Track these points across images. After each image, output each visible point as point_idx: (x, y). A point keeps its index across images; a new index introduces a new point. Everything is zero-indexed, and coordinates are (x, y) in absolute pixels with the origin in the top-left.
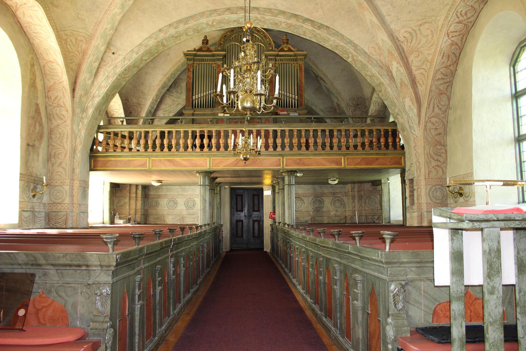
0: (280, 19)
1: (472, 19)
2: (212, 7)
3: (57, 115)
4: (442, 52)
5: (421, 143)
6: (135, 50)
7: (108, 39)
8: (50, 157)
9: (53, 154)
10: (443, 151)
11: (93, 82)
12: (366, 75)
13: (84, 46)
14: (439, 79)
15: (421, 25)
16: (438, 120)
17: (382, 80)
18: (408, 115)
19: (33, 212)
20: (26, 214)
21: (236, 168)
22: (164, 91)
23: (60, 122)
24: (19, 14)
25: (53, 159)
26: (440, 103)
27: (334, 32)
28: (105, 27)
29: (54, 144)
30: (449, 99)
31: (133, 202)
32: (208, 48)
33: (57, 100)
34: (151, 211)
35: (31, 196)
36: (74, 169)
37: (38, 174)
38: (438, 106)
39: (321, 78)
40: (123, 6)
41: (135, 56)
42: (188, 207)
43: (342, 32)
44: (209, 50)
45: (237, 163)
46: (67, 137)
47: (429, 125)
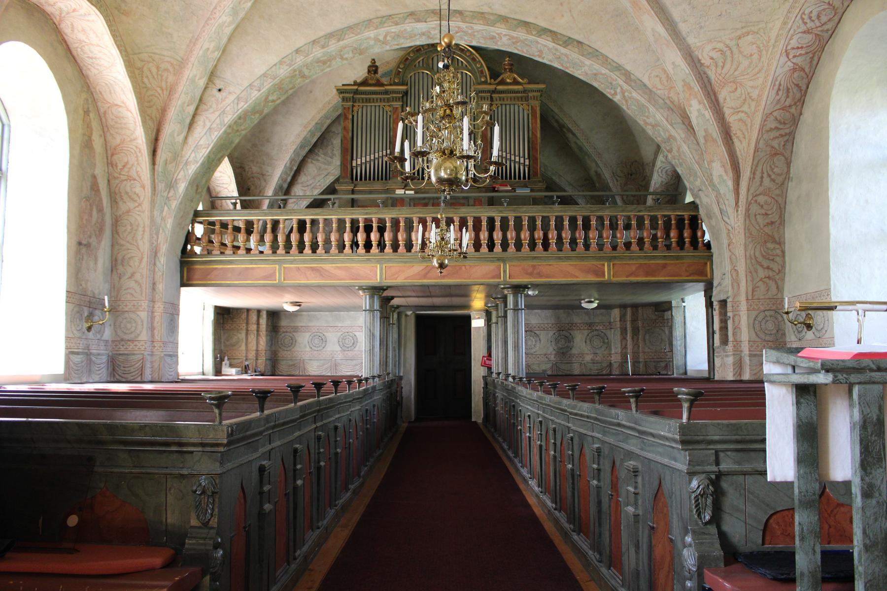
0: (499, 31)
1: (829, 26)
2: (384, 11)
3: (127, 193)
4: (777, 83)
5: (739, 239)
6: (255, 84)
7: (210, 66)
8: (115, 264)
9: (120, 258)
10: (778, 252)
11: (186, 138)
12: (646, 123)
13: (171, 79)
14: (771, 130)
15: (740, 38)
16: (769, 200)
17: (673, 132)
18: (718, 191)
19: (88, 355)
20: (76, 359)
21: (426, 281)
22: (304, 153)
23: (132, 205)
24: (65, 28)
25: (120, 267)
26: (772, 170)
27: (591, 50)
28: (204, 48)
29: (123, 242)
30: (788, 164)
31: (252, 338)
32: (378, 80)
33: (126, 169)
34: (283, 354)
35: (85, 329)
36: (154, 284)
37: (96, 292)
38: (769, 176)
39: (569, 130)
40: (235, 11)
41: (255, 95)
42: (344, 347)
43: (605, 51)
44: (379, 83)
45: (427, 274)
46: (144, 231)
47: (754, 208)
